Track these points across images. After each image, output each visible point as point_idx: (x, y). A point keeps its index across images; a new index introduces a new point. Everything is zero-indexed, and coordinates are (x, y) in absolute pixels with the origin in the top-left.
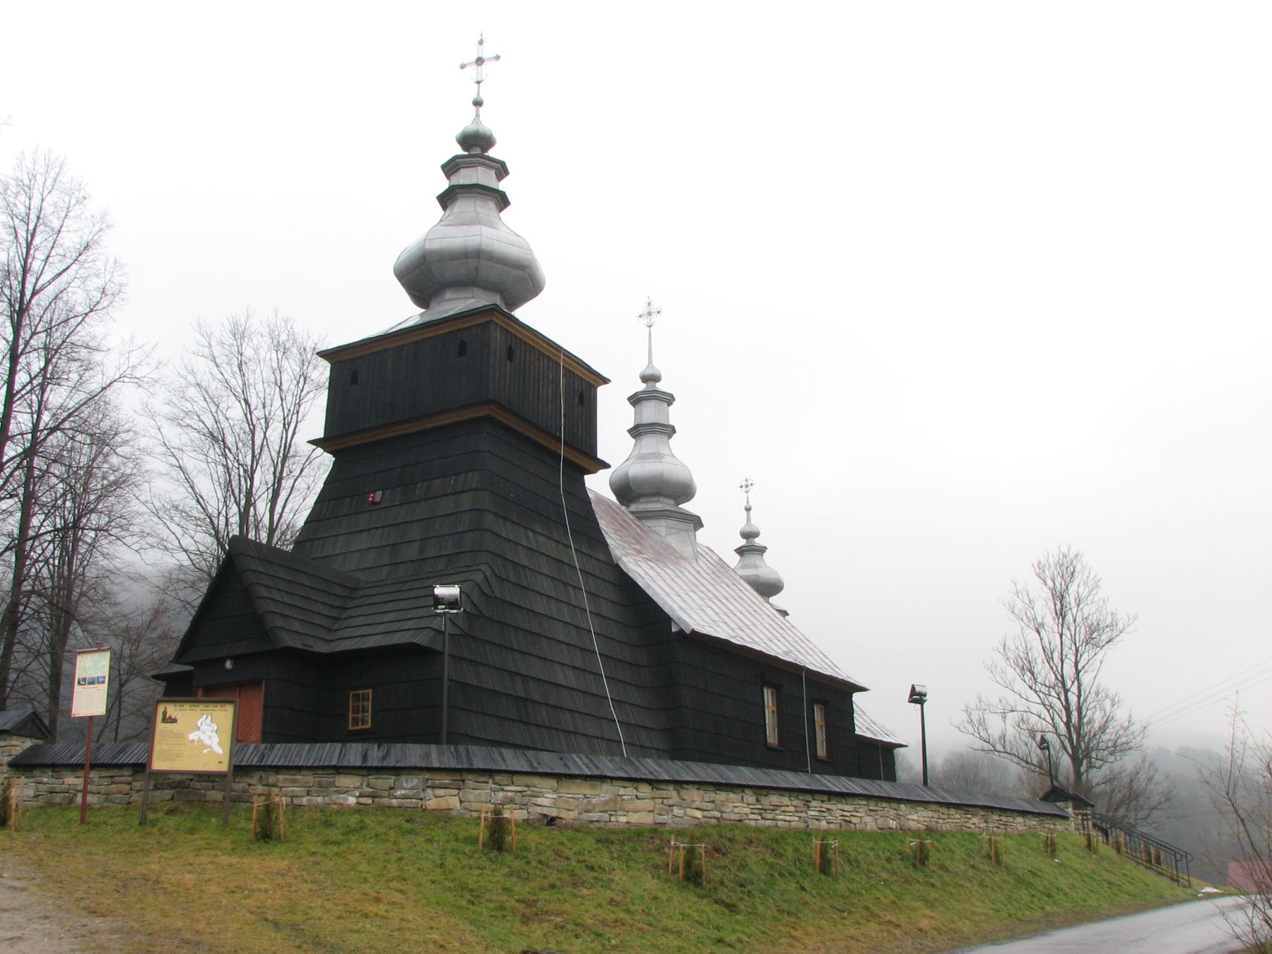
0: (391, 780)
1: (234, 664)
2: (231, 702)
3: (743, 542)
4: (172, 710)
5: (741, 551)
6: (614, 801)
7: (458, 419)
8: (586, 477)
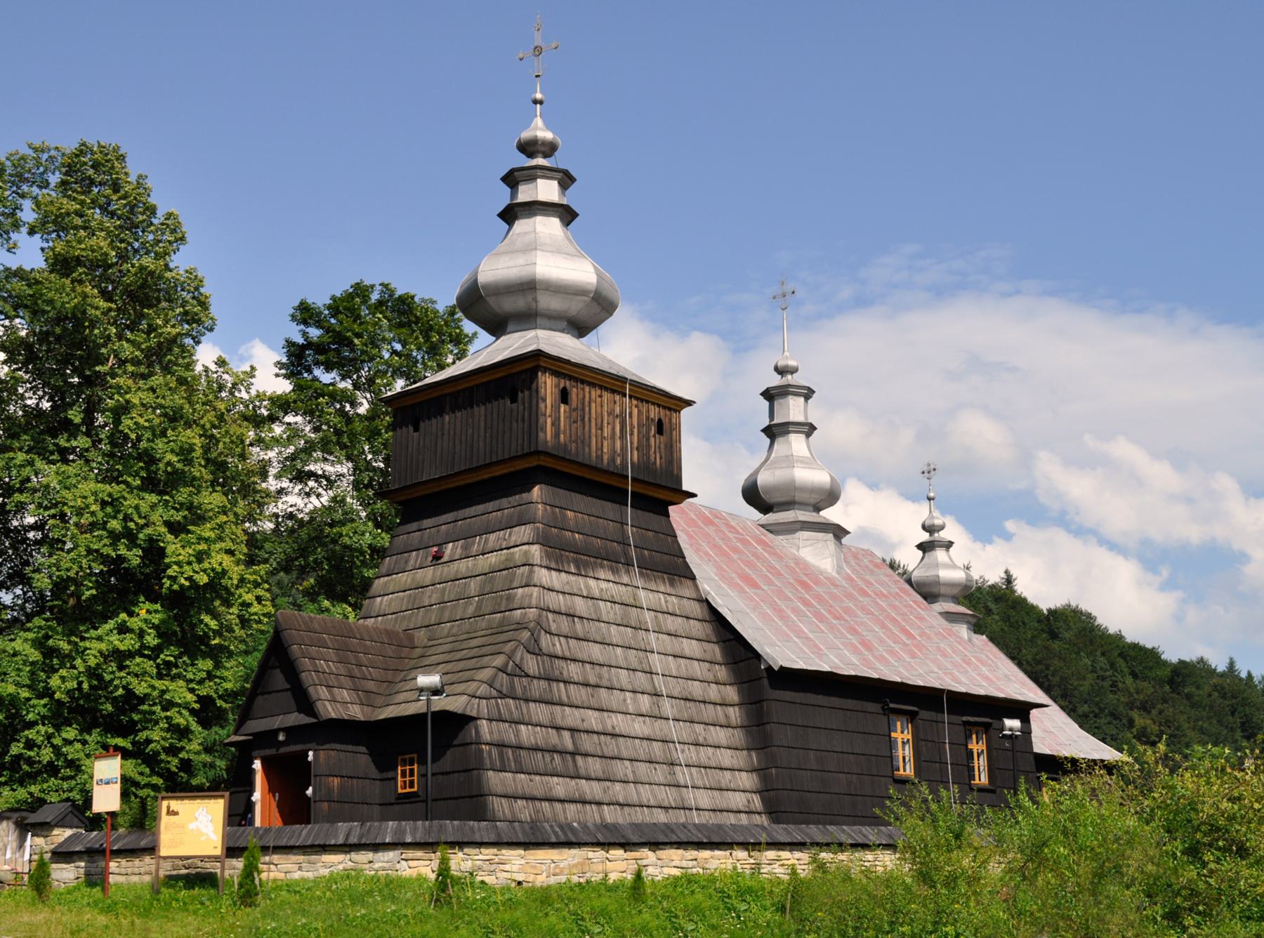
0: (370, 855)
1: (287, 736)
2: (222, 797)
3: (925, 537)
4: (175, 805)
5: (924, 547)
6: (582, 864)
7: (512, 469)
8: (671, 508)
